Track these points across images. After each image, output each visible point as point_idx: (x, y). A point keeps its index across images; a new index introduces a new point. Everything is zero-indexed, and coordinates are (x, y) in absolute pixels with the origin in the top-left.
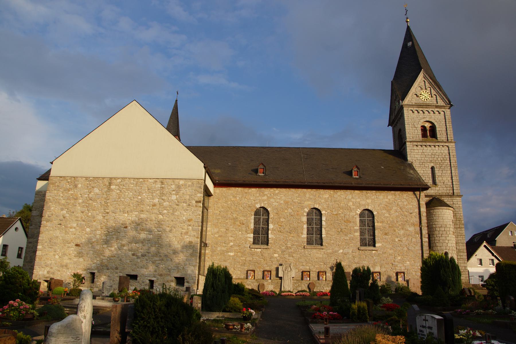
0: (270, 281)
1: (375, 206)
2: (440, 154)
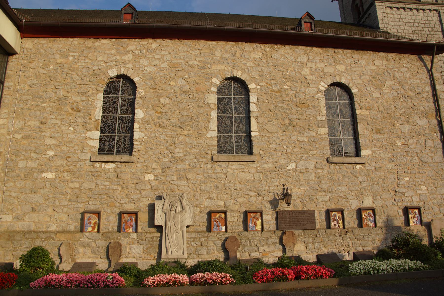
0: (134, 235)
1: (354, 78)
2: (427, 22)
